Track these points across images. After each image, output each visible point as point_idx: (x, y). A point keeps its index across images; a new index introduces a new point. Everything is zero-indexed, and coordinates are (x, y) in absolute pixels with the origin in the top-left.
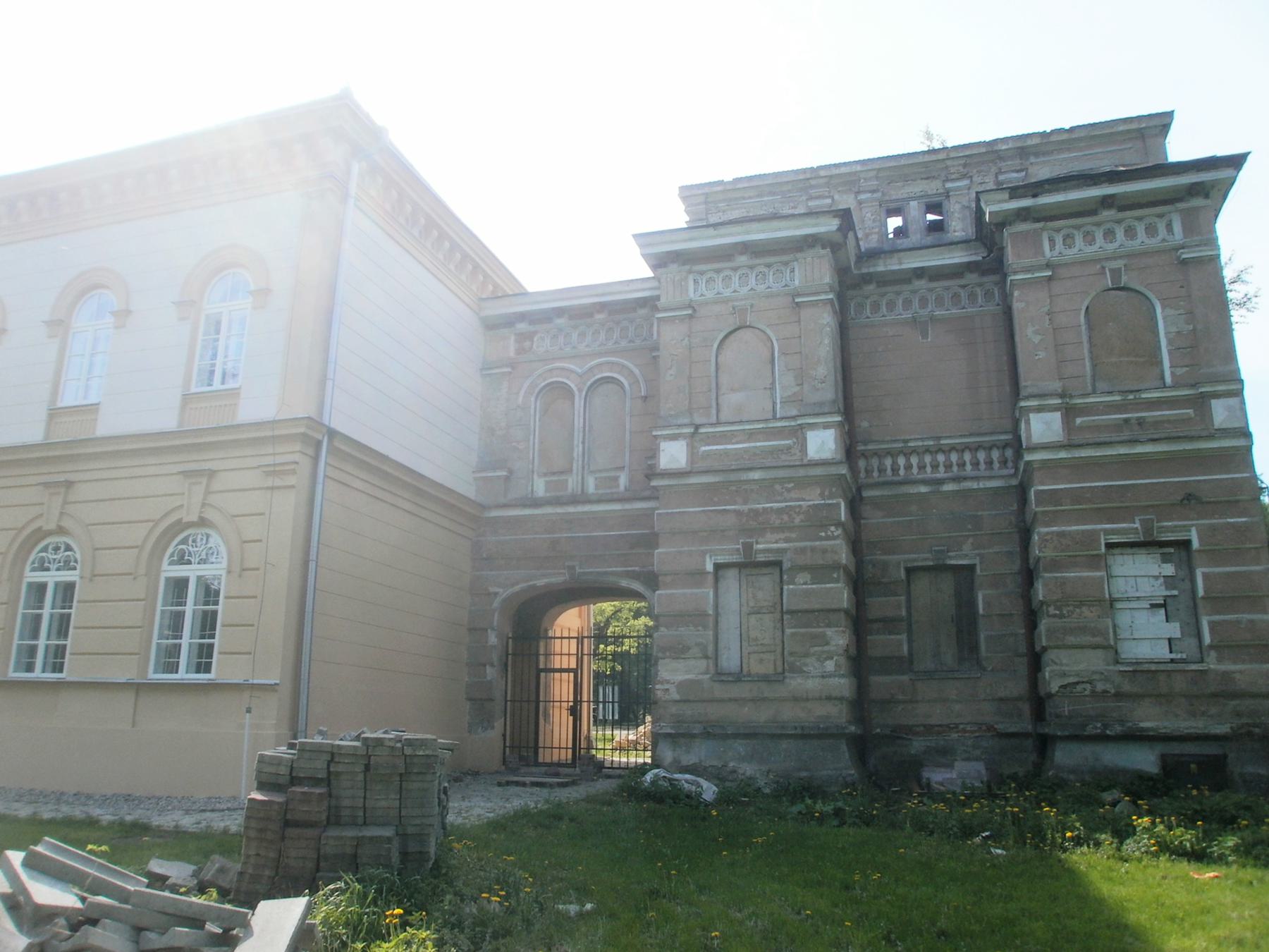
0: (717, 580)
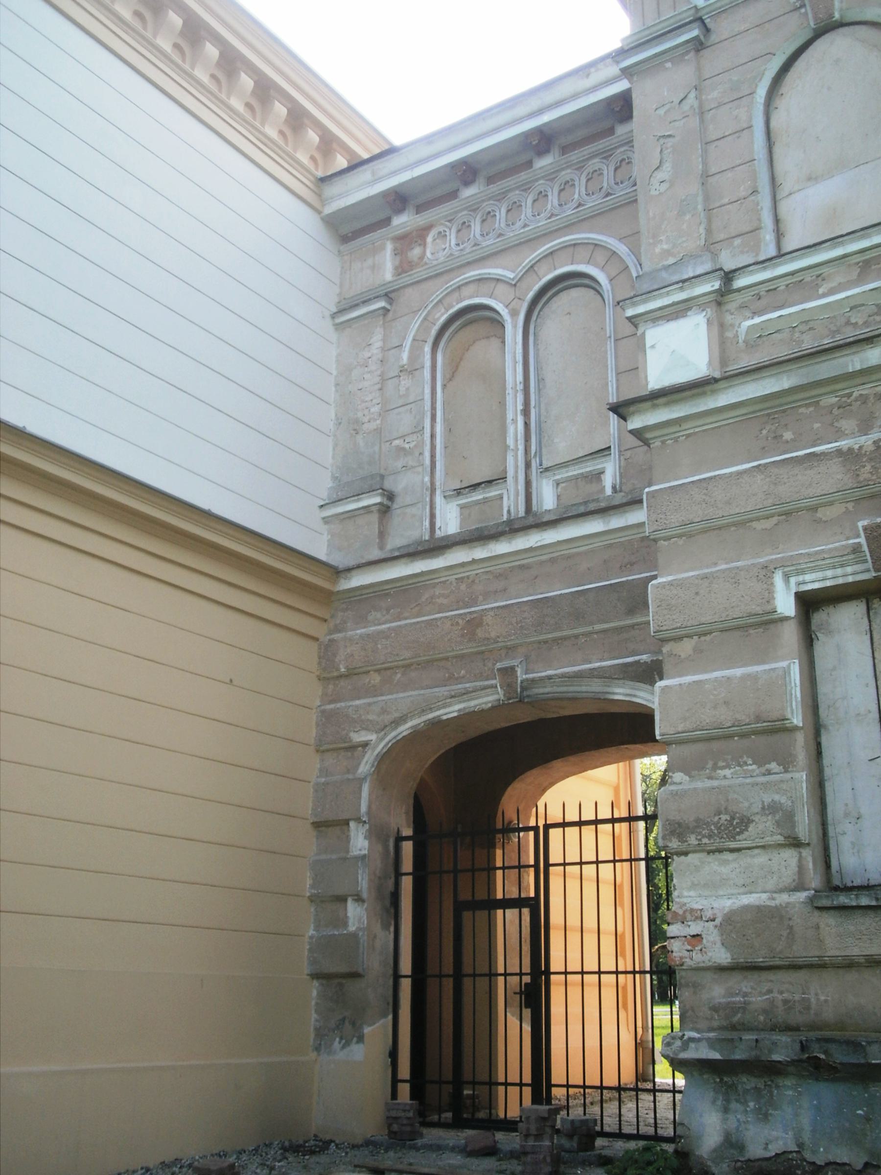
0: (809, 640)
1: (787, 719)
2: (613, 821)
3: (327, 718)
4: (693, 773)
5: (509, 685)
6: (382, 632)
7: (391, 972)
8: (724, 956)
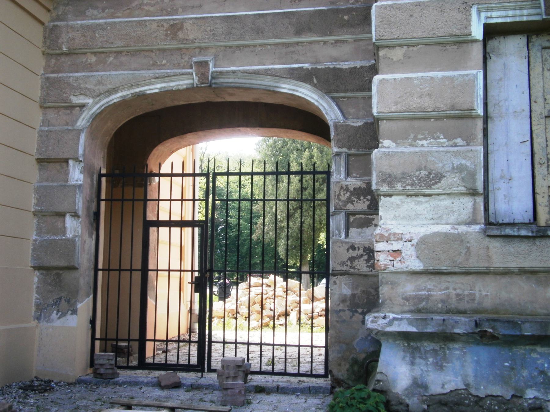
1: (474, 110)
2: (183, 175)
3: (50, 84)
4: (399, 141)
5: (203, 74)
6: (100, 25)
7: (92, 266)
8: (417, 265)
